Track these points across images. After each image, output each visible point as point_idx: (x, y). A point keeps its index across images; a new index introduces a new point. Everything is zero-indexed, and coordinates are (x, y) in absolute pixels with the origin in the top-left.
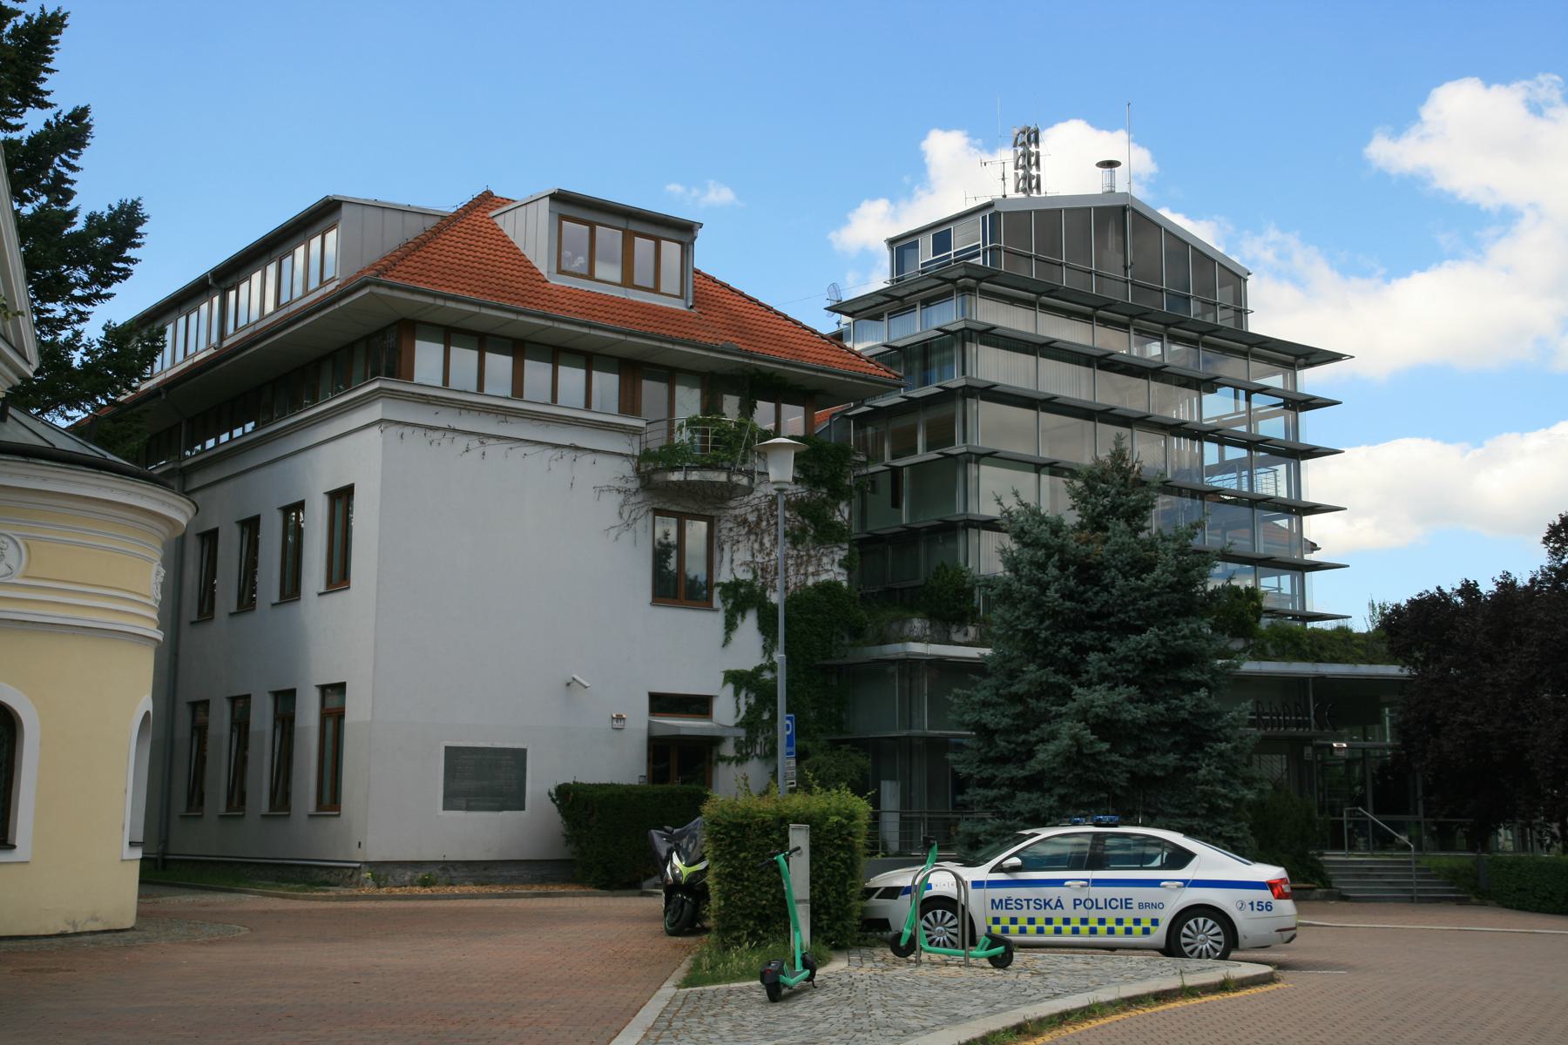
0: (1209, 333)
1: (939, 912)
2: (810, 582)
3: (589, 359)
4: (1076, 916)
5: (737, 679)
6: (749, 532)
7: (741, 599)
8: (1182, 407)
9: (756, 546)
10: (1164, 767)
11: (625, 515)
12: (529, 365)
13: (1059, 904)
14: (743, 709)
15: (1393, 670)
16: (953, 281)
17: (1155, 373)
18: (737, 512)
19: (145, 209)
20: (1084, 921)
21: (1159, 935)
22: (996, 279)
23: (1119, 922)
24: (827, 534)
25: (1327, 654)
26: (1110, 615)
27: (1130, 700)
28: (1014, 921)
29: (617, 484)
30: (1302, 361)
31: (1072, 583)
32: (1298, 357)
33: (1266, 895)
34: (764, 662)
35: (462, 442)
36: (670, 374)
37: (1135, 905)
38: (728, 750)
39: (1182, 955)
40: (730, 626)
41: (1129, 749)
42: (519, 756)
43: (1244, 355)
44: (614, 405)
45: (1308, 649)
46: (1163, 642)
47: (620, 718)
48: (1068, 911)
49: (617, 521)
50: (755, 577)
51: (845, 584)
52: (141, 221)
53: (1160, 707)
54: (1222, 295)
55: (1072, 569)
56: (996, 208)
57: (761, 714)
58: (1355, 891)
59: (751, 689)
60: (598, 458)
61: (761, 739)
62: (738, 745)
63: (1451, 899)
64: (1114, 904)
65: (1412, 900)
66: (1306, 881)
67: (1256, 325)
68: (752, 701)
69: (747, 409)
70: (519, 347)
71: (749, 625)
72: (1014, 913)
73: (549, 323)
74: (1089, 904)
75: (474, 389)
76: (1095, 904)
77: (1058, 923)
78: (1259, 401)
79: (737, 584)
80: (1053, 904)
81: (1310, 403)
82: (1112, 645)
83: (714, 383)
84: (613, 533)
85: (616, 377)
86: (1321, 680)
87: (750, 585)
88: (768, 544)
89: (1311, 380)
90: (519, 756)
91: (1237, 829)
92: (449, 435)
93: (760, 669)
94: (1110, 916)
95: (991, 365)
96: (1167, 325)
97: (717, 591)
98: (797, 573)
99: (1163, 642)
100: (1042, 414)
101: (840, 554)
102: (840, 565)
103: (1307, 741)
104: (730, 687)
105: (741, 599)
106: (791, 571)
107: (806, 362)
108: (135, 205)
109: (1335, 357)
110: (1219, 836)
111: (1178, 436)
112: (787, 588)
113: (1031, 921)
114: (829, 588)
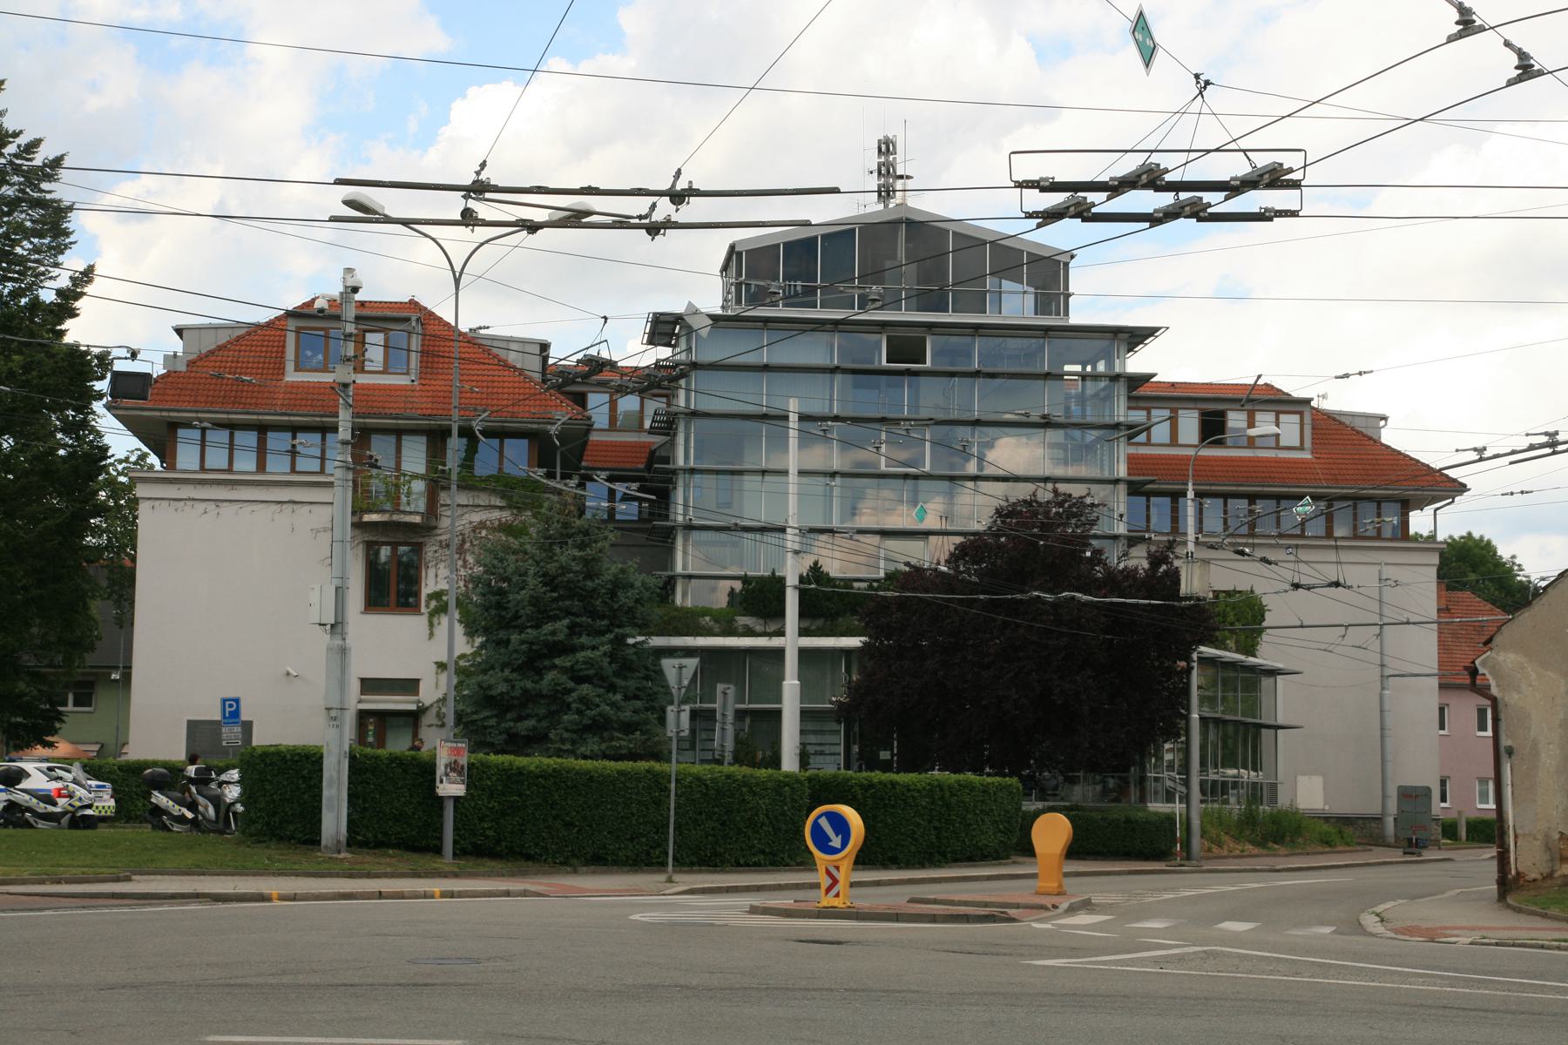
9: (460, 563)
18: (443, 538)
35: (201, 507)
60: (314, 507)
75: (197, 468)
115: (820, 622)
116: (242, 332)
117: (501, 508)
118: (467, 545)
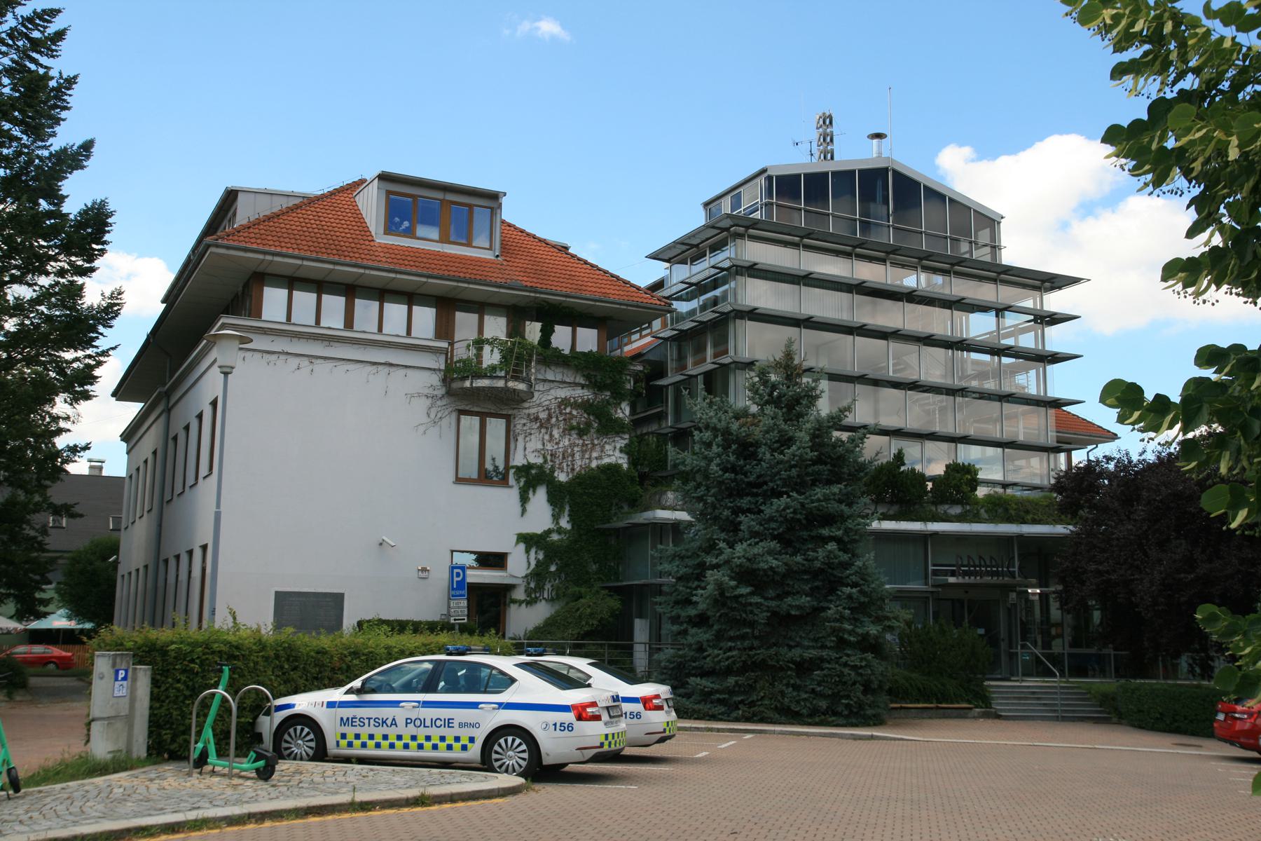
0: (958, 264)
1: (306, 730)
2: (594, 464)
3: (411, 297)
4: (407, 732)
5: (528, 540)
6: (541, 426)
7: (531, 478)
8: (937, 322)
9: (547, 437)
10: (798, 607)
11: (432, 416)
12: (359, 303)
13: (394, 723)
14: (533, 563)
15: (1060, 529)
16: (727, 229)
17: (911, 297)
18: (532, 411)
19: (111, 207)
20: (414, 738)
21: (475, 752)
22: (759, 226)
23: (443, 739)
24: (609, 427)
25: (1029, 517)
26: (765, 483)
27: (770, 552)
28: (357, 736)
29: (426, 391)
30: (1047, 284)
31: (732, 458)
32: (1043, 281)
33: (570, 717)
34: (552, 526)
35: (294, 362)
36: (481, 307)
37: (456, 724)
38: (519, 594)
39: (492, 770)
40: (524, 499)
41: (771, 593)
42: (338, 599)
43: (994, 280)
44: (430, 333)
45: (1013, 513)
46: (803, 505)
47: (424, 570)
48: (401, 729)
49: (425, 419)
50: (546, 461)
51: (625, 466)
52: (111, 214)
53: (799, 558)
54: (984, 236)
55: (734, 447)
56: (769, 173)
57: (548, 567)
58: (1010, 711)
59: (539, 548)
60: (409, 371)
61: (548, 586)
62: (528, 591)
63: (1089, 718)
64: (438, 723)
65: (1057, 719)
66: (970, 702)
67: (1009, 257)
68: (541, 556)
69: (547, 333)
70: (351, 290)
71: (540, 497)
72: (358, 730)
73: (362, 271)
74: (418, 723)
75: (284, 320)
76: (423, 723)
77: (392, 739)
78: (1011, 320)
79: (529, 467)
80: (389, 722)
81: (1054, 319)
82: (763, 508)
83: (517, 314)
84: (422, 429)
85: (434, 310)
86: (1020, 537)
87: (541, 467)
88: (557, 436)
89: (1054, 301)
90: (338, 599)
91: (861, 659)
92: (283, 357)
93: (549, 532)
94: (435, 733)
95: (757, 294)
96: (921, 259)
97: (512, 471)
98: (582, 458)
99: (803, 505)
100: (857, 338)
101: (621, 442)
102: (621, 451)
103: (1011, 588)
104: (522, 546)
105: (531, 478)
106: (577, 456)
107: (583, 295)
108: (103, 204)
109: (1074, 281)
110: (610, 662)
111: (962, 350)
112: (573, 469)
113: (371, 737)
114: (612, 469)
115: (896, 508)
116: (297, 201)
117: (583, 387)
118: (554, 420)
